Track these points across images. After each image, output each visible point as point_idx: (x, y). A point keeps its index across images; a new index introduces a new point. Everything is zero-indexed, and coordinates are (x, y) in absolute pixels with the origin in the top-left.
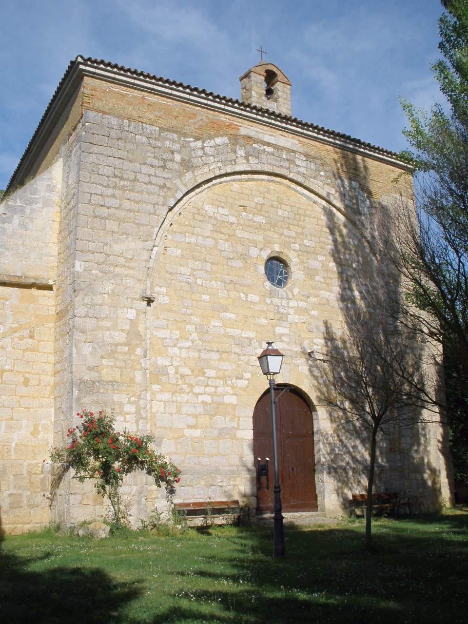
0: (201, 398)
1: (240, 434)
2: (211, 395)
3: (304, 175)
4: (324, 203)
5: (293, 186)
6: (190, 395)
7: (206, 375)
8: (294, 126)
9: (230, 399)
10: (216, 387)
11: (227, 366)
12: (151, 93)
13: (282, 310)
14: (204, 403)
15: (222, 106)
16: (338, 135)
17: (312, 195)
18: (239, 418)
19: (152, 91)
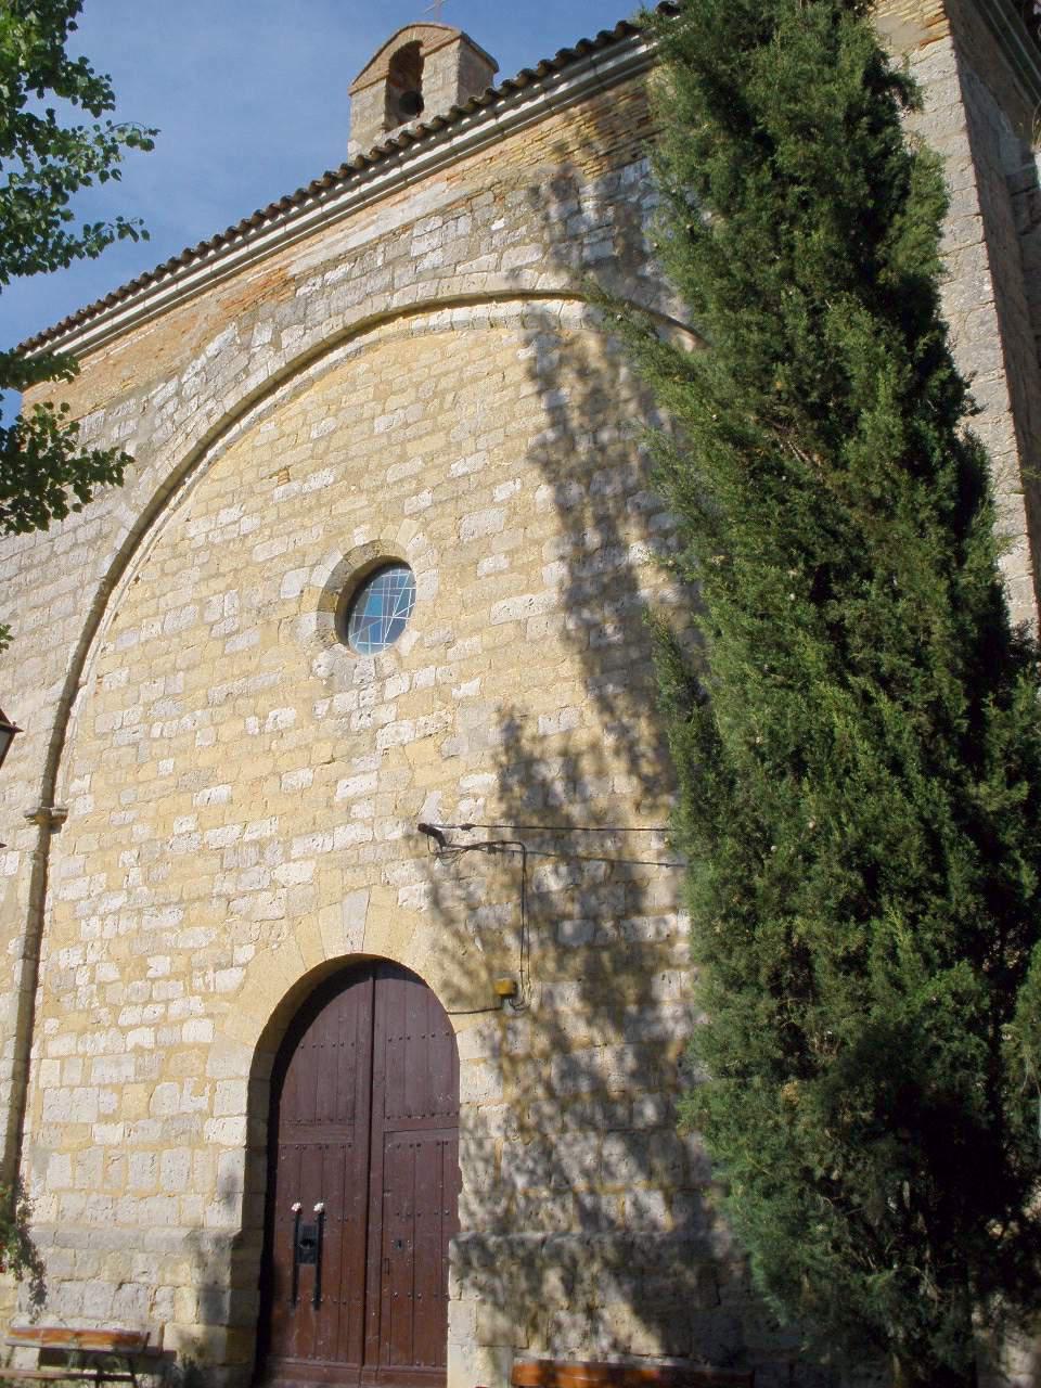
0: (133, 1038)
1: (212, 1130)
2: (156, 1026)
3: (436, 274)
4: (516, 306)
5: (418, 321)
6: (113, 1031)
7: (151, 973)
8: (419, 152)
9: (198, 1031)
10: (167, 1002)
11: (198, 937)
12: (120, 336)
13: (356, 723)
14: (139, 1050)
15: (243, 251)
16: (548, 68)
17: (480, 310)
18: (214, 1082)
19: (118, 332)
